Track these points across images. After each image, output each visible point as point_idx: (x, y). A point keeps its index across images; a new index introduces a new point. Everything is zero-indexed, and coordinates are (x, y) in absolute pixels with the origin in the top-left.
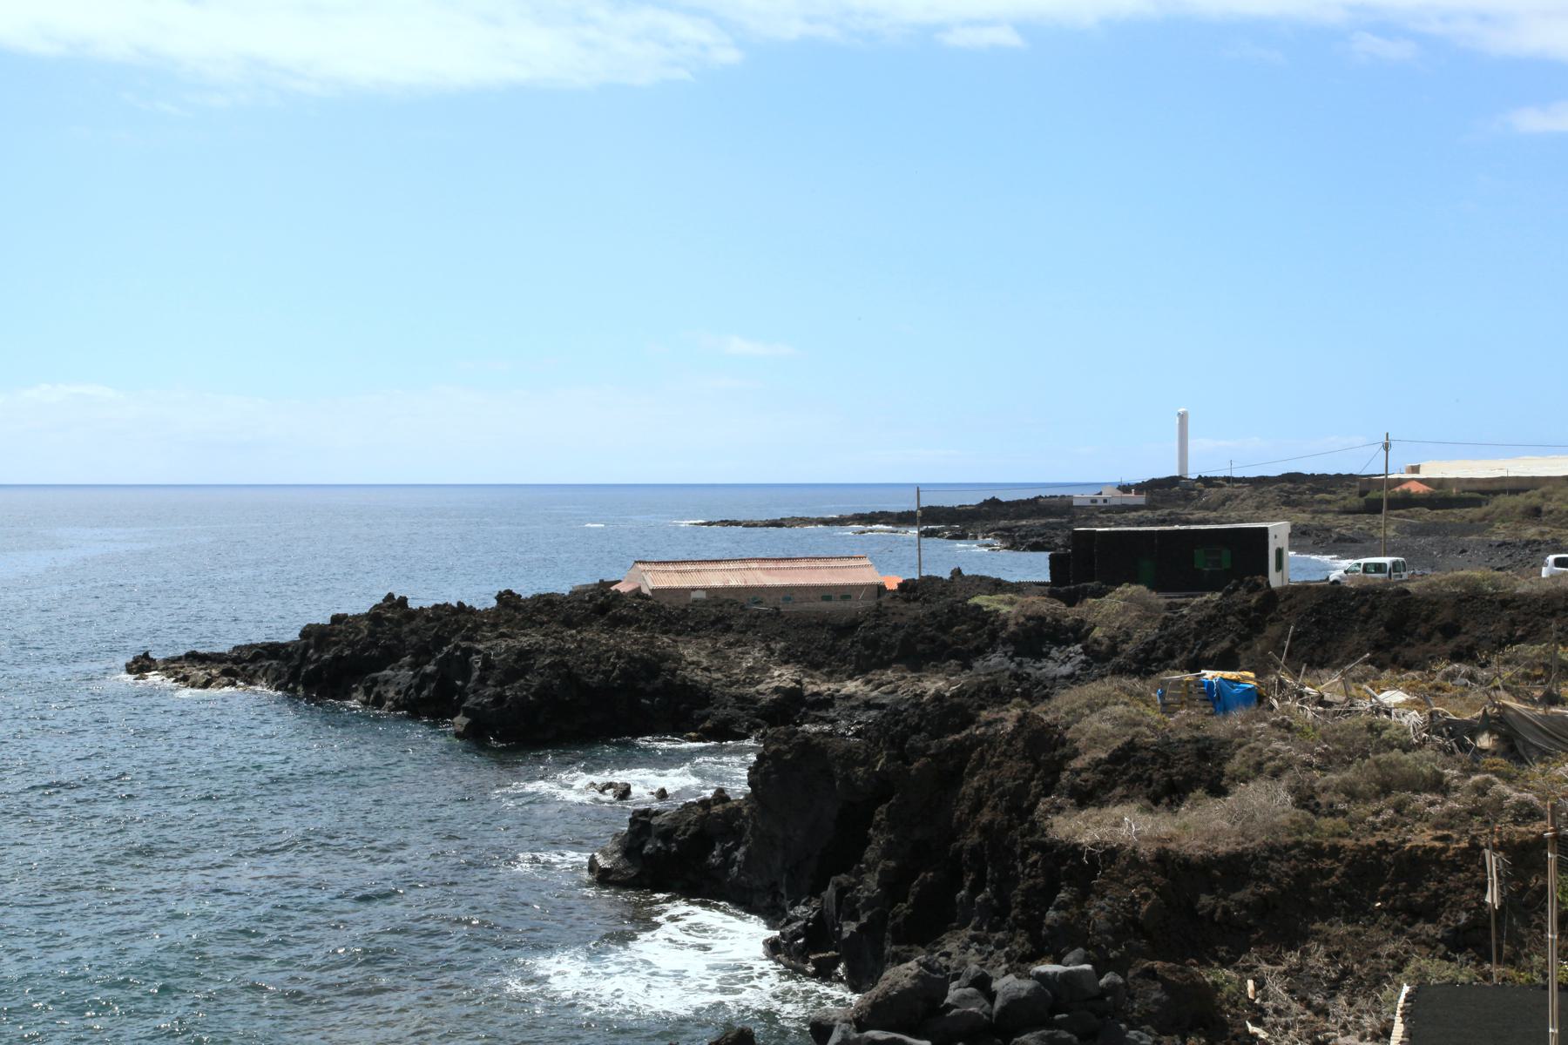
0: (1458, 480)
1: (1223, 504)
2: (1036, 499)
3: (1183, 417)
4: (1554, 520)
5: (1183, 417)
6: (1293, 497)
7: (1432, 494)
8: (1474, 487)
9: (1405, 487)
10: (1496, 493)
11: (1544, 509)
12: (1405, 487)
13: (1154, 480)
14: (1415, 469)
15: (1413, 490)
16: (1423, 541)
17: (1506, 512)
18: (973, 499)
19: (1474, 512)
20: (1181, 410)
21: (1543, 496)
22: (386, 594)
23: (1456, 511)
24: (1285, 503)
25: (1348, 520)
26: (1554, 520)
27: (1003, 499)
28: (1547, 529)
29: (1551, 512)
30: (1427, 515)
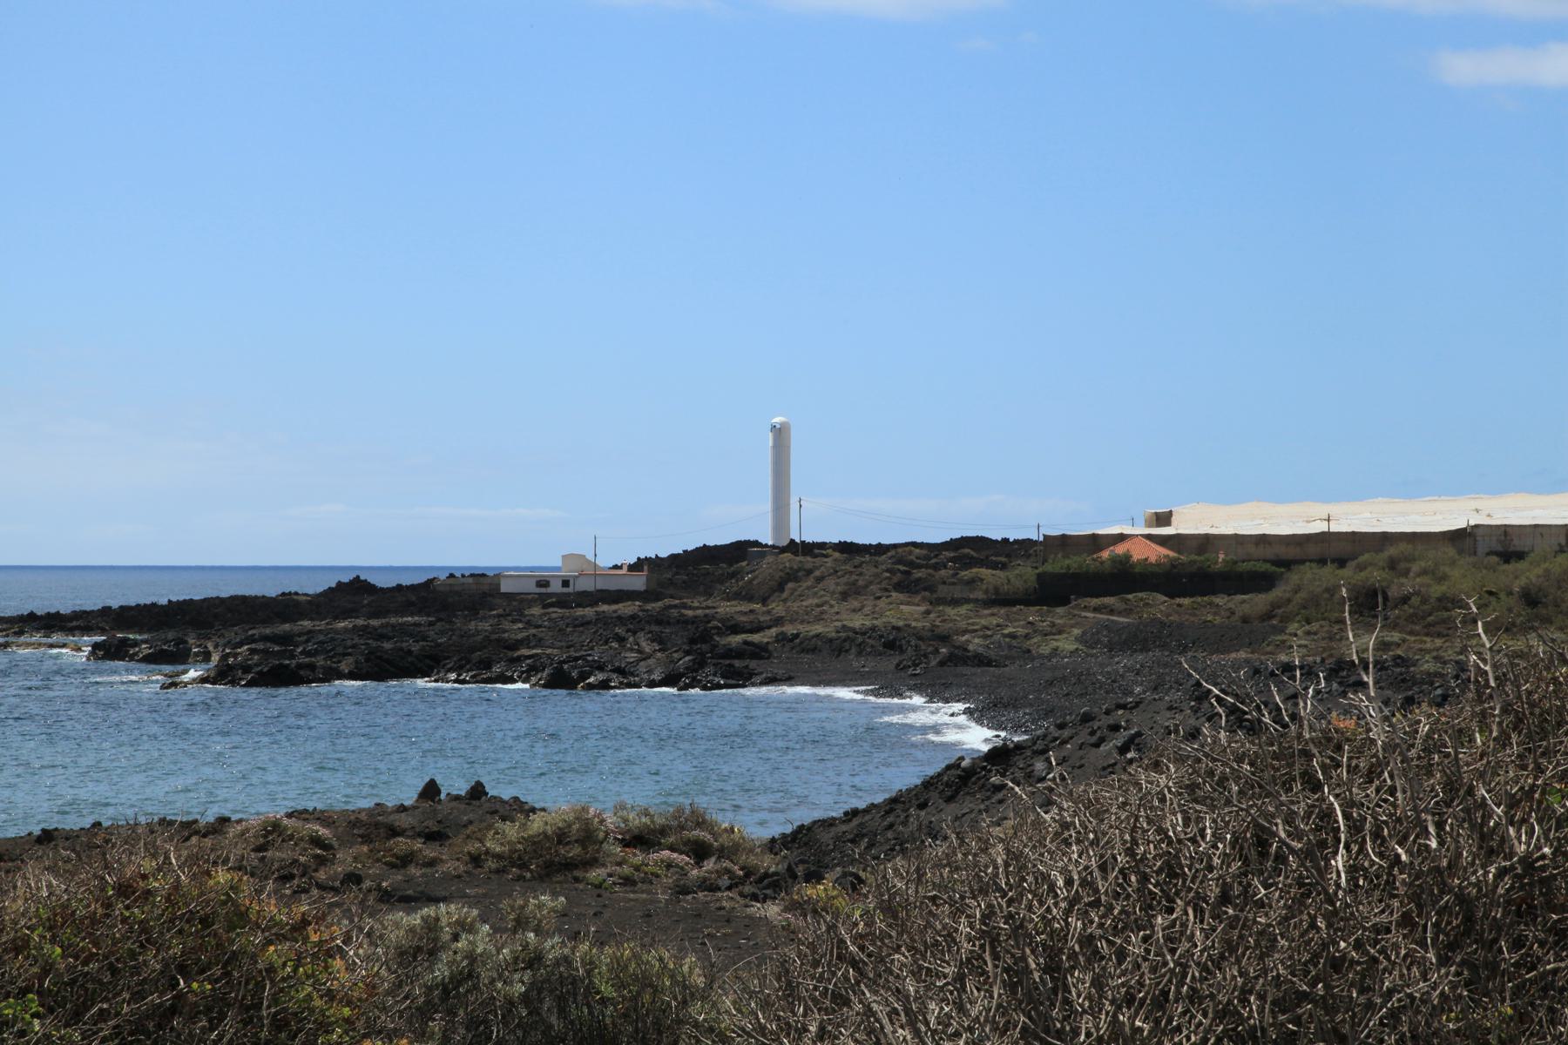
0: (1238, 539)
1: (781, 587)
2: (430, 581)
3: (780, 434)
4: (1412, 619)
5: (780, 434)
6: (918, 574)
7: (1173, 564)
8: (1270, 553)
9: (1120, 549)
10: (1287, 564)
11: (1393, 592)
12: (1120, 549)
13: (705, 549)
14: (1163, 519)
15: (1137, 556)
16: (1123, 661)
17: (1314, 601)
18: (315, 586)
19: (1254, 603)
20: (777, 420)
21: (1392, 565)
22: (427, 779)
23: (1220, 600)
24: (899, 587)
25: (991, 618)
26: (1412, 619)
27: (380, 585)
28: (1395, 636)
29: (1405, 600)
30: (1159, 605)
